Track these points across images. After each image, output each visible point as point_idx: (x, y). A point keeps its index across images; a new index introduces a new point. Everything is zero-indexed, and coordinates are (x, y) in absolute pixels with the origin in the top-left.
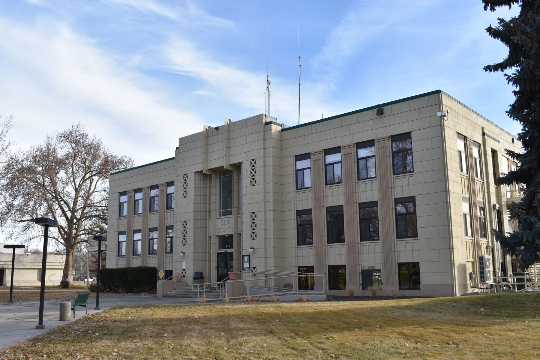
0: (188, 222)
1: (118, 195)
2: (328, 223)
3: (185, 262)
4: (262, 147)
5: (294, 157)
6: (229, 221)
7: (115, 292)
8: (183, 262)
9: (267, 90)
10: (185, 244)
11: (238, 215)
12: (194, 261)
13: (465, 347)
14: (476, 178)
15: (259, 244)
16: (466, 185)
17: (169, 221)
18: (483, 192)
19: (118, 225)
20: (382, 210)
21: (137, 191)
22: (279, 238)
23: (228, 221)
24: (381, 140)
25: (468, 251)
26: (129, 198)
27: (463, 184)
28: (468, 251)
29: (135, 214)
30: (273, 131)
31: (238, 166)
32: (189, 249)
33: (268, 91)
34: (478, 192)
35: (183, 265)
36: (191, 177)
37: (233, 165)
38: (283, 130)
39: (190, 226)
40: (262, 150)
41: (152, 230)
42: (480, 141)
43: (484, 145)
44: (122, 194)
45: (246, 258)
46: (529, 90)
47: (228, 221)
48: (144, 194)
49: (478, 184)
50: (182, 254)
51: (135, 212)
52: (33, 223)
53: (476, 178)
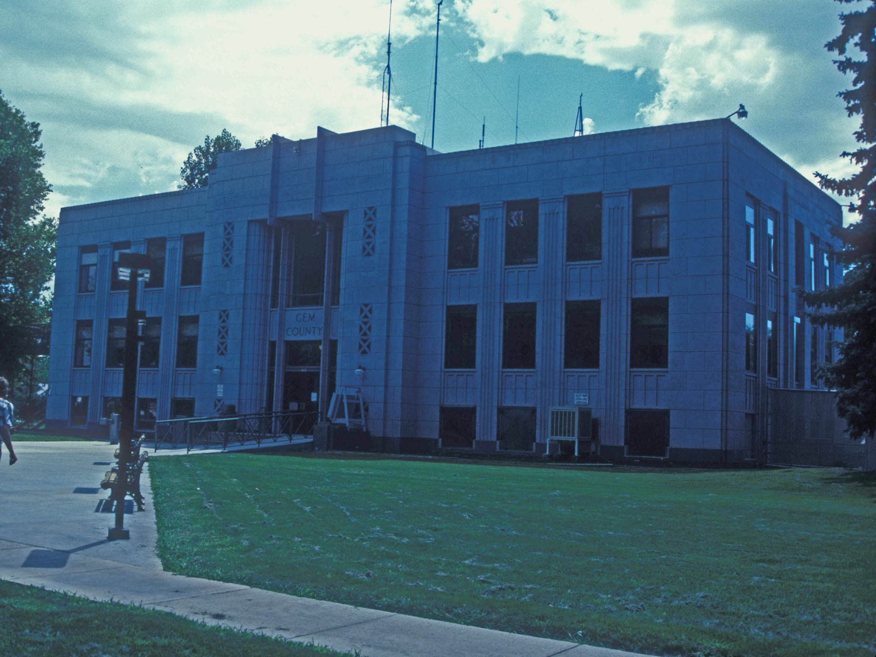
3: (222, 386)
5: (448, 210)
6: (312, 316)
8: (219, 386)
9: (387, 70)
10: (224, 352)
11: (288, 309)
14: (768, 271)
16: (753, 284)
18: (778, 296)
20: (606, 389)
23: (310, 315)
25: (748, 395)
27: (749, 282)
28: (748, 395)
33: (389, 73)
34: (770, 295)
35: (219, 390)
37: (328, 216)
42: (779, 208)
43: (786, 215)
47: (310, 315)
49: (770, 281)
50: (219, 370)
53: (768, 271)
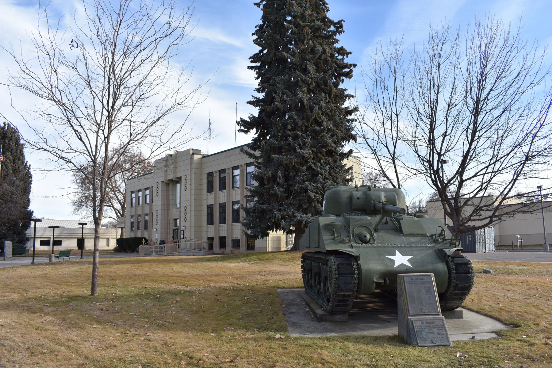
0: (158, 211)
1: (130, 193)
2: (220, 212)
4: (190, 168)
7: (126, 252)
12: (161, 234)
13: (134, 271)
15: (187, 224)
17: (234, 196)
19: (131, 211)
21: (139, 191)
22: (198, 220)
24: (242, 165)
26: (142, 193)
29: (233, 187)
30: (195, 159)
31: (180, 178)
32: (159, 227)
36: (160, 184)
38: (203, 158)
39: (159, 213)
40: (190, 170)
41: (146, 215)
44: (132, 192)
45: (182, 232)
46: (92, 194)
48: (241, 171)
51: (139, 204)
52: (426, 143)
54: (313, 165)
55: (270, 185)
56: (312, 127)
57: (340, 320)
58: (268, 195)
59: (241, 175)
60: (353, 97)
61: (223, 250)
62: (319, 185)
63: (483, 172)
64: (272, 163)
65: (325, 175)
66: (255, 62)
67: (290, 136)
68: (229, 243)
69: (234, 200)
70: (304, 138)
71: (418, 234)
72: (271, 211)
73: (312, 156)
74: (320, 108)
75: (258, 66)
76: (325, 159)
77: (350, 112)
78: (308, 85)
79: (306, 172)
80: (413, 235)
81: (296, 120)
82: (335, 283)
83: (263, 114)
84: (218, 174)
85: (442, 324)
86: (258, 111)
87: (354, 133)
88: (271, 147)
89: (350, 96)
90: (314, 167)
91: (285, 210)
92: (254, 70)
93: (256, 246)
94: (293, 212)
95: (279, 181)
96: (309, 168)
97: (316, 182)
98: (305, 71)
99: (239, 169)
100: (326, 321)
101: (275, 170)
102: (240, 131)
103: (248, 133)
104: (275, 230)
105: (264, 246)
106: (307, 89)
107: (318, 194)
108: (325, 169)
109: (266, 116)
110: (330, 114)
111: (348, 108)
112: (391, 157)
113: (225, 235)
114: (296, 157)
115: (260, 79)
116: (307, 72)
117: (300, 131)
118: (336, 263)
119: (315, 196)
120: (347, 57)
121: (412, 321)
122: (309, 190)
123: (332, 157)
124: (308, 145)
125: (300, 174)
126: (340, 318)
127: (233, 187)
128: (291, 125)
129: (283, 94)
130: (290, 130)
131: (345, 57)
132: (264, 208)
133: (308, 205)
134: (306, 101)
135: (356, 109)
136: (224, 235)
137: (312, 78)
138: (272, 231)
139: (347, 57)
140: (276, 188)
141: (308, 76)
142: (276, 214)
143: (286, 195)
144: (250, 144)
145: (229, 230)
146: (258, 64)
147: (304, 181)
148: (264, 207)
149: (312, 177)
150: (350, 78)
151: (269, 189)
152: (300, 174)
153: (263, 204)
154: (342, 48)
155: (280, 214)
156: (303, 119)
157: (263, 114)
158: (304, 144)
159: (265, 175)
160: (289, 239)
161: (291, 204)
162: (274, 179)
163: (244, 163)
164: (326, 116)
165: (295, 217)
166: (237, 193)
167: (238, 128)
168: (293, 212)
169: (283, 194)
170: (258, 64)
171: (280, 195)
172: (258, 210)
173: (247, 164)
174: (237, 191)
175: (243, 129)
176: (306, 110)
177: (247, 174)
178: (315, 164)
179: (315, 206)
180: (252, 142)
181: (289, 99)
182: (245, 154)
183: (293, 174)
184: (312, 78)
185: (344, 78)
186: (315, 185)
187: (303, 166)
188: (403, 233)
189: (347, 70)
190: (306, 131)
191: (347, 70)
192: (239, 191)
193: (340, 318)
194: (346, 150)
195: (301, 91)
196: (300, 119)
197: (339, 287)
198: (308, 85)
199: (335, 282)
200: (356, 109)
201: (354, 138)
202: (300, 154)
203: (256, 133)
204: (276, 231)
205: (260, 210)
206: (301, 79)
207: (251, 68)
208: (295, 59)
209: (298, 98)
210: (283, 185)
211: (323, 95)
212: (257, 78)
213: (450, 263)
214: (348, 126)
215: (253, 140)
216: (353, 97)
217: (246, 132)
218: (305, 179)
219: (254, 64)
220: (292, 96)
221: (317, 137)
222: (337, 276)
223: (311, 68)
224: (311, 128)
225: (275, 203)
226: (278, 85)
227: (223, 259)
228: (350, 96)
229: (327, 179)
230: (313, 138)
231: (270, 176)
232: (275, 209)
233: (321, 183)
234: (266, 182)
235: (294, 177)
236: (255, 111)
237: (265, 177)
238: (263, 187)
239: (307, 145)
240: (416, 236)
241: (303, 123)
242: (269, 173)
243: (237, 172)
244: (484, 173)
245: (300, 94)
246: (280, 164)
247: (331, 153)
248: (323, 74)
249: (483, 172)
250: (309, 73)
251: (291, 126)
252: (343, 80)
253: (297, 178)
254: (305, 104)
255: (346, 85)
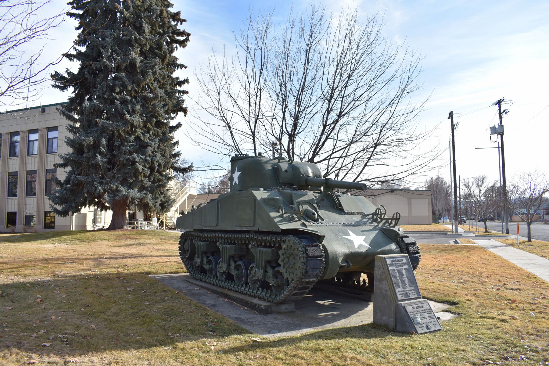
17: (11, 166)
29: (28, 154)
48: (40, 136)
54: (142, 135)
55: (90, 155)
56: (143, 93)
57: (286, 311)
58: (87, 165)
59: (40, 140)
60: (186, 67)
61: (11, 227)
62: (148, 158)
63: (329, 158)
64: (93, 128)
65: (154, 147)
66: (77, 9)
67: (118, 100)
68: (20, 220)
69: (29, 169)
70: (134, 104)
71: (357, 213)
72: (91, 183)
73: (142, 125)
74: (154, 73)
75: (80, 15)
76: (155, 130)
77: (181, 83)
78: (142, 46)
79: (133, 142)
80: (353, 214)
81: (126, 83)
82: (303, 268)
83: (86, 70)
84: (8, 137)
85: (429, 308)
86: (79, 66)
87: (184, 106)
88: (94, 109)
89: (182, 66)
90: (142, 138)
91: (107, 184)
92: (74, 18)
93: (56, 224)
94: (117, 187)
95: (103, 149)
96: (138, 138)
97: (144, 154)
98: (140, 29)
99: (38, 133)
100: (271, 313)
101: (98, 137)
102: (54, 86)
103: (65, 90)
104: (87, 206)
105: (68, 224)
106: (140, 51)
107: (145, 167)
108: (155, 141)
109: (89, 74)
110: (162, 81)
111: (178, 78)
112: (251, 133)
113: (16, 210)
114: (124, 124)
115: (82, 29)
116: (142, 31)
117: (129, 96)
118: (302, 245)
119: (143, 169)
120: (181, 24)
121: (404, 307)
122: (136, 162)
123: (161, 128)
124: (138, 112)
125: (126, 144)
126: (287, 309)
127: (28, 154)
128: (119, 87)
129: (113, 51)
130: (118, 93)
131: (179, 24)
132: (83, 179)
133: (134, 179)
134: (139, 63)
135: (186, 81)
136: (13, 211)
137: (146, 39)
138: (84, 206)
139: (181, 24)
140: (99, 157)
141: (143, 35)
142: (96, 188)
143: (109, 166)
144: (66, 103)
145: (21, 205)
146: (80, 12)
147: (131, 153)
148: (82, 178)
149: (139, 148)
150: (184, 46)
151: (89, 159)
152: (126, 144)
153: (80, 174)
154: (178, 13)
155: (102, 187)
156: (133, 83)
157: (86, 70)
158: (134, 111)
159: (86, 141)
160: (97, 217)
161: (114, 177)
162: (96, 146)
163: (25, 129)
164: (157, 83)
165: (120, 191)
166: (33, 161)
167: (53, 83)
168: (117, 187)
169: (105, 165)
170: (80, 12)
171: (103, 166)
172: (73, 182)
173: (48, 128)
174: (33, 159)
175: (59, 84)
176: (137, 73)
177: (48, 139)
178: (143, 134)
179: (142, 181)
180: (68, 101)
181: (119, 57)
182: (62, 115)
183: (118, 144)
184: (146, 39)
185: (178, 46)
186: (143, 157)
187: (130, 135)
188: (344, 212)
189: (181, 38)
190: (135, 97)
191: (181, 38)
192: (37, 159)
193: (287, 309)
194: (173, 123)
195: (133, 51)
196: (130, 81)
197: (307, 272)
198: (142, 46)
199: (303, 267)
200: (186, 81)
201: (185, 111)
202: (129, 121)
203: (74, 92)
204: (89, 206)
205: (76, 182)
206: (135, 37)
207: (71, 15)
208: (128, 14)
209: (129, 59)
210: (106, 155)
211: (158, 59)
212: (78, 28)
213: (402, 243)
214: (178, 98)
215: (69, 99)
216: (186, 67)
217: (63, 89)
218: (132, 150)
219: (75, 11)
220: (123, 55)
221: (147, 105)
222: (305, 260)
223: (147, 28)
224: (141, 94)
225: (95, 175)
226: (107, 39)
227: (28, 239)
228: (182, 66)
229: (155, 151)
230: (142, 106)
231: (92, 143)
232: (95, 181)
233: (149, 156)
234: (86, 150)
235: (119, 147)
236: (75, 67)
237: (86, 144)
238: (82, 155)
239: (136, 112)
240: (356, 215)
241: (133, 88)
242: (91, 140)
243: (17, 138)
244: (339, 156)
245: (133, 54)
246: (104, 129)
247: (159, 124)
248: (159, 37)
249: (329, 158)
250: (144, 32)
251: (120, 89)
252: (177, 47)
253: (124, 148)
254: (138, 66)
255: (179, 53)
